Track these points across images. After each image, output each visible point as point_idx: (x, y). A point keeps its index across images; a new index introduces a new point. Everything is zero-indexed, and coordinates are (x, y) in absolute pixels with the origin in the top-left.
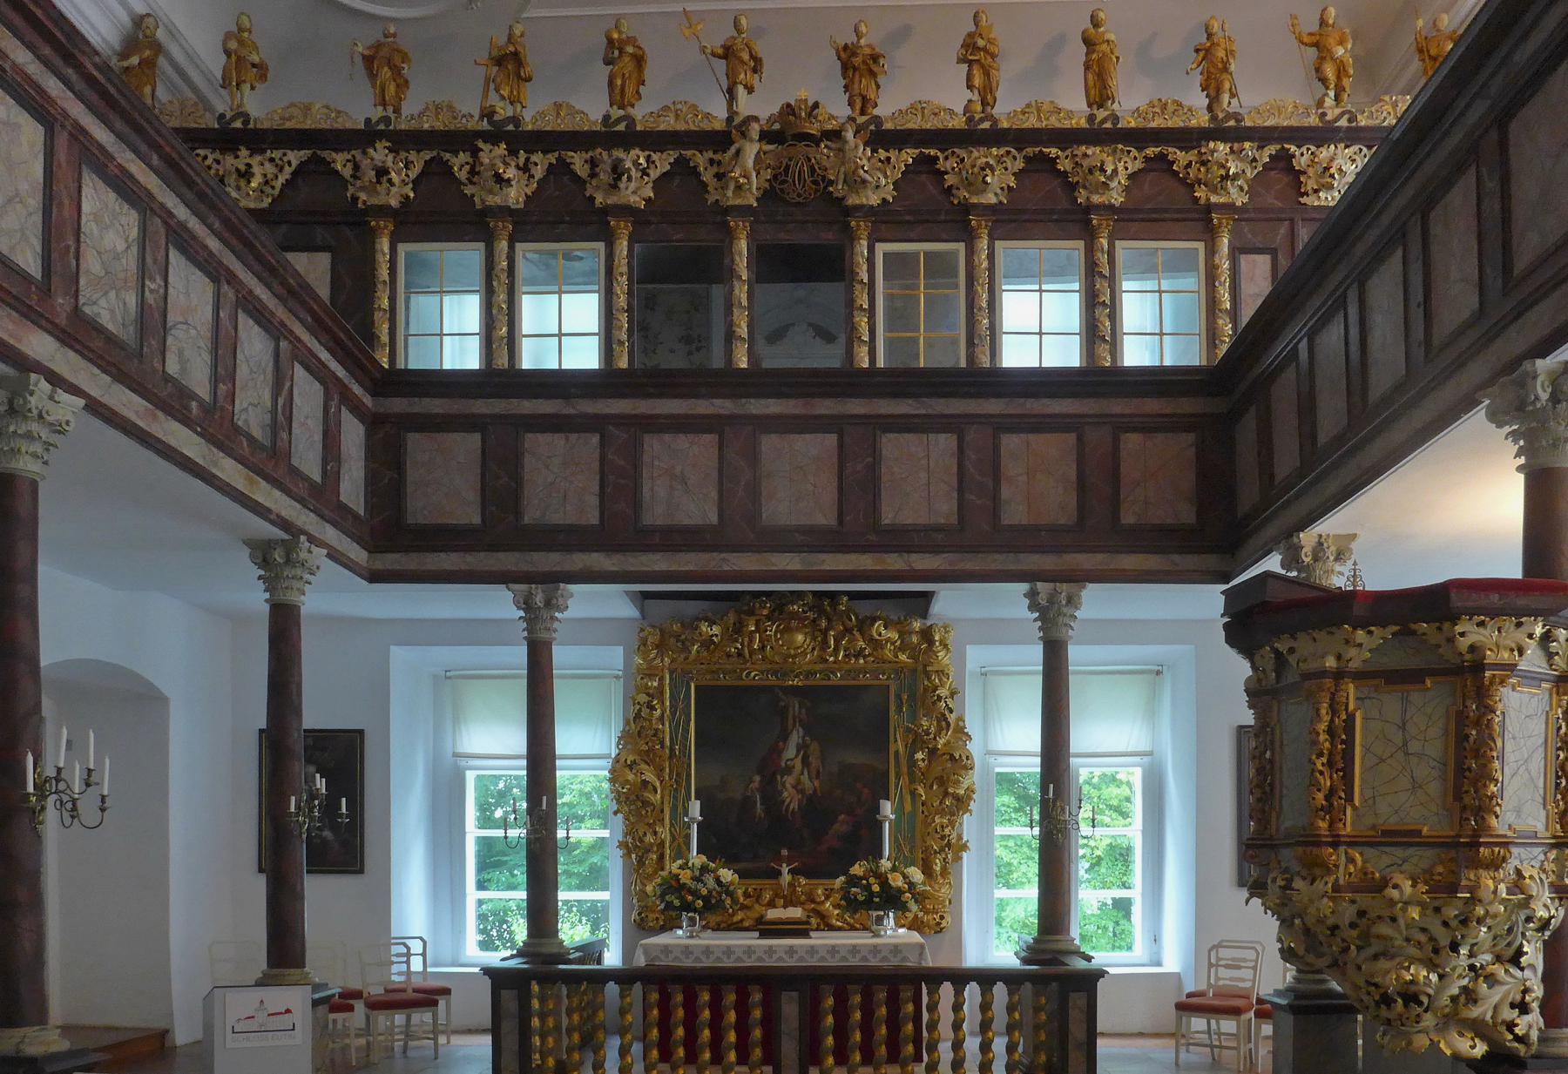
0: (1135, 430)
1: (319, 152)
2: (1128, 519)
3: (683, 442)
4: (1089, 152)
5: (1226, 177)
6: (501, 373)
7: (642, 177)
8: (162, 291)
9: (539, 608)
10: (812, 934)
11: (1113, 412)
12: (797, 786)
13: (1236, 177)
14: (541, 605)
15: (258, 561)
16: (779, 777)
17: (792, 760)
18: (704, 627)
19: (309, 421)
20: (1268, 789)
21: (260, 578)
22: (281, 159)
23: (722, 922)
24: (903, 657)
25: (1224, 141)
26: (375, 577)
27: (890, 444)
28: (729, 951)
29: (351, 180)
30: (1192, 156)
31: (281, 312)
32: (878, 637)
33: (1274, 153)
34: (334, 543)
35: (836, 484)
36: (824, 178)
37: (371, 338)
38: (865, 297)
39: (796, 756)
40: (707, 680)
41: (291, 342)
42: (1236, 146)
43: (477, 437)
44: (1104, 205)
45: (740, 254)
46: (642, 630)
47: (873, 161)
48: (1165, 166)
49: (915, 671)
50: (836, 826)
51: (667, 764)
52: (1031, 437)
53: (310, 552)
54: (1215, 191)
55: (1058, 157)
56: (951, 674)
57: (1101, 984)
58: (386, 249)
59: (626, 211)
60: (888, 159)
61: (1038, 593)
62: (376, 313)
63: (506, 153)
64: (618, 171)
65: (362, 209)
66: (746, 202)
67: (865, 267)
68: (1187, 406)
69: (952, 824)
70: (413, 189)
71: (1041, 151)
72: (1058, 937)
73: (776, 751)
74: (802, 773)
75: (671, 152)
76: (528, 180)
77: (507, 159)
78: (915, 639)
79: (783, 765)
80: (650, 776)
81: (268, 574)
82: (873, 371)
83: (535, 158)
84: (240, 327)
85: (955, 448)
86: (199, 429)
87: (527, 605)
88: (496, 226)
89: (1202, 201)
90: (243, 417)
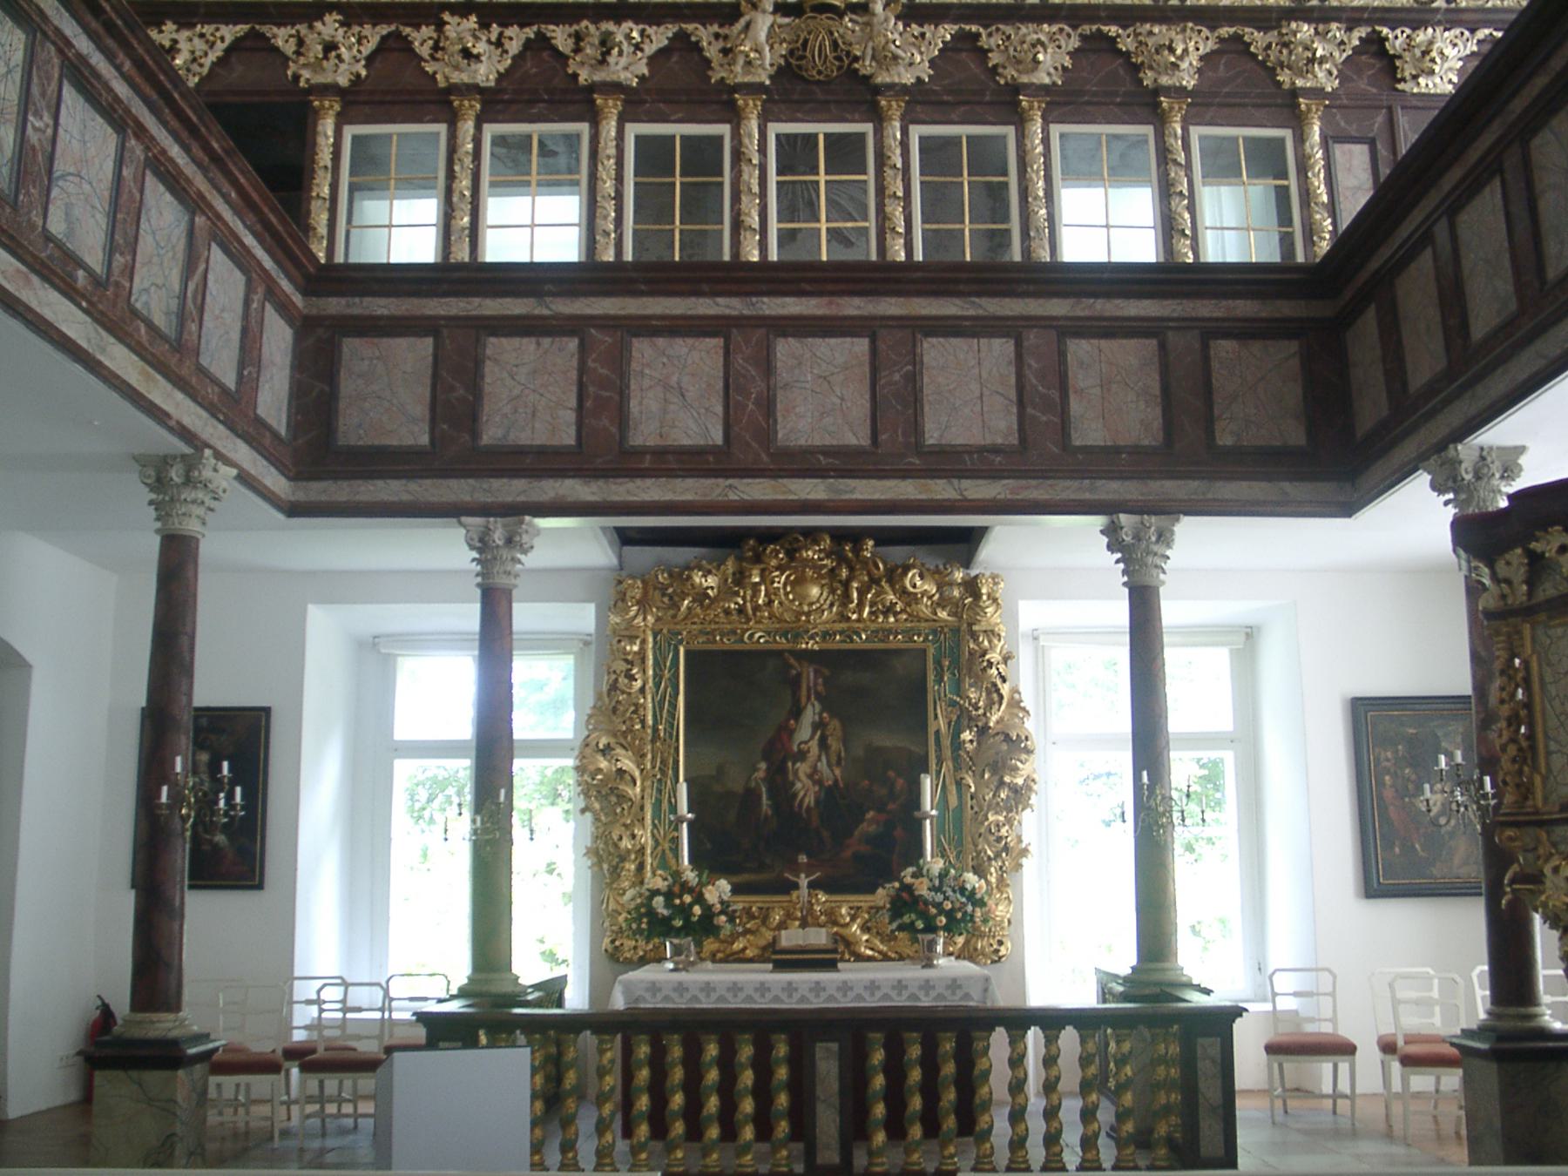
0: (1227, 335)
1: (257, 27)
2: (1225, 439)
3: (680, 346)
4: (1156, 30)
5: (1312, 60)
6: (461, 266)
7: (634, 53)
8: (50, 131)
9: (498, 546)
10: (840, 965)
11: (1200, 315)
12: (813, 774)
13: (1322, 60)
14: (500, 543)
15: (149, 481)
16: (790, 764)
17: (806, 743)
18: (697, 578)
19: (225, 315)
20: (1524, 744)
21: (151, 503)
22: (212, 35)
23: (718, 951)
24: (943, 614)
25: (1308, 21)
26: (294, 510)
27: (934, 351)
28: (735, 988)
29: (294, 57)
30: (1272, 36)
31: (200, 183)
32: (911, 590)
33: (1364, 35)
34: (247, 465)
35: (867, 397)
36: (848, 53)
37: (307, 229)
38: (899, 183)
39: (812, 738)
40: (699, 644)
41: (209, 218)
42: (1321, 27)
43: (429, 342)
44: (1175, 87)
45: (750, 136)
46: (620, 582)
47: (907, 35)
48: (1241, 47)
49: (958, 630)
50: (864, 826)
51: (649, 747)
52: (1104, 343)
53: (215, 470)
54: (1301, 74)
55: (1118, 36)
56: (1003, 634)
57: (1238, 1025)
58: (330, 133)
59: (615, 88)
60: (923, 35)
61: (1122, 528)
62: (313, 203)
63: (476, 26)
64: (606, 44)
65: (304, 89)
66: (757, 80)
67: (898, 151)
68: (1286, 308)
69: (1009, 821)
70: (366, 66)
71: (1099, 30)
72: (1160, 965)
73: (784, 732)
74: (819, 759)
75: (670, 26)
76: (501, 56)
77: (477, 33)
78: (956, 593)
79: (795, 748)
80: (627, 764)
81: (161, 497)
82: (909, 265)
83: (510, 32)
84: (147, 192)
85: (1012, 355)
86: (84, 304)
87: (482, 545)
88: (461, 105)
89: (1286, 86)
90: (144, 298)
